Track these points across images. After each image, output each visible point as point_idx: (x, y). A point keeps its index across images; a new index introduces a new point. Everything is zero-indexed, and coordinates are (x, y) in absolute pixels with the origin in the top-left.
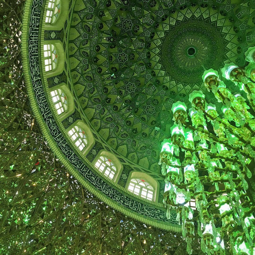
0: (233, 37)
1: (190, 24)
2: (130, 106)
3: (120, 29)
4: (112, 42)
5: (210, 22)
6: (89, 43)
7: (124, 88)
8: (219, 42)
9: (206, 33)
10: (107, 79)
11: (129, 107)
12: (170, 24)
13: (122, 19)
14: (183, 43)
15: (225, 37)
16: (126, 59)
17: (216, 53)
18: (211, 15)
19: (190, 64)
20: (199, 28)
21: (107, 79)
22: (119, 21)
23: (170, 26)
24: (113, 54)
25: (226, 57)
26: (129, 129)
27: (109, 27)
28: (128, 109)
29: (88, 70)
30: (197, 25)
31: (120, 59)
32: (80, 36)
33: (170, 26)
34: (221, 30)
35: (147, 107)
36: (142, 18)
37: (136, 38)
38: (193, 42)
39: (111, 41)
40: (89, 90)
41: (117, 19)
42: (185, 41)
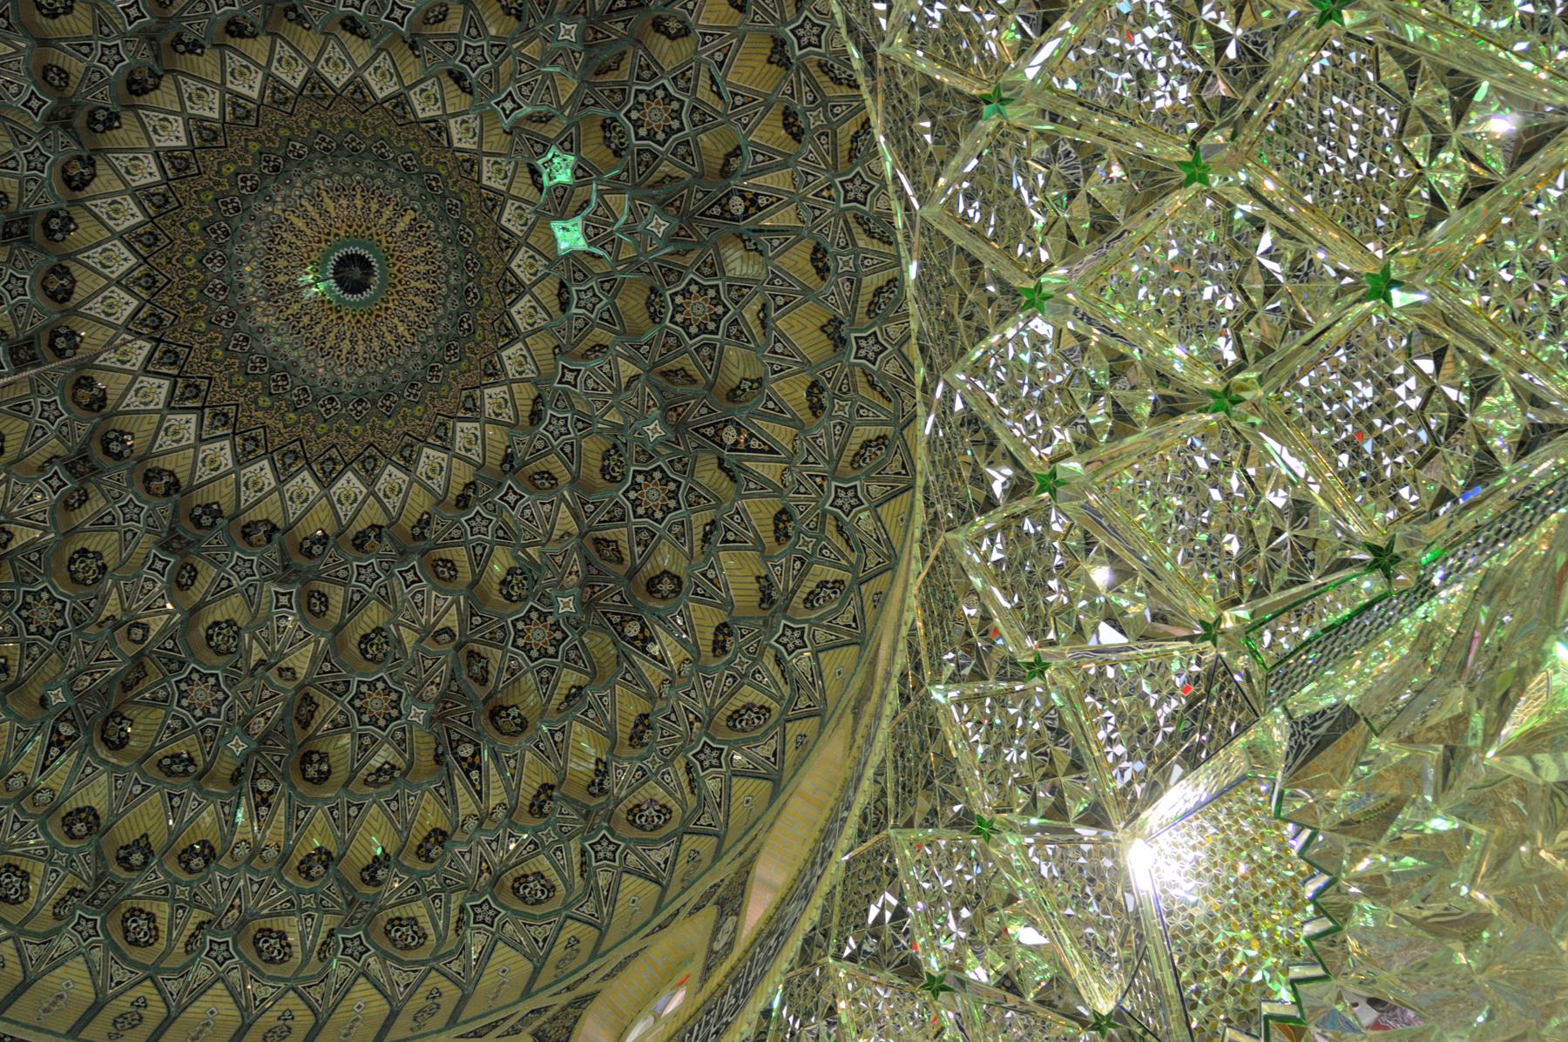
0: (90, 253)
1: (281, 425)
2: (734, 218)
3: (586, 640)
4: (640, 619)
5: (176, 383)
6: (737, 703)
7: (734, 330)
8: (185, 254)
9: (236, 329)
10: (772, 451)
11: (746, 215)
12: (365, 491)
13: (546, 681)
14: (376, 345)
15: (131, 270)
16: (657, 475)
17: (225, 204)
18: (156, 417)
19: (387, 213)
20: (256, 378)
21: (772, 451)
22: (569, 678)
23: (370, 479)
24: (691, 549)
25: (167, 165)
26: (792, 95)
27: (613, 697)
28: (760, 209)
29: (832, 574)
30: (255, 401)
31: (673, 495)
32: (365, 975)
33: (370, 479)
34: (141, 315)
35: (662, 144)
36: (439, 626)
37: (398, 630)
38: (324, 322)
39: (643, 627)
40: (869, 478)
41: (568, 697)
42: (361, 348)
